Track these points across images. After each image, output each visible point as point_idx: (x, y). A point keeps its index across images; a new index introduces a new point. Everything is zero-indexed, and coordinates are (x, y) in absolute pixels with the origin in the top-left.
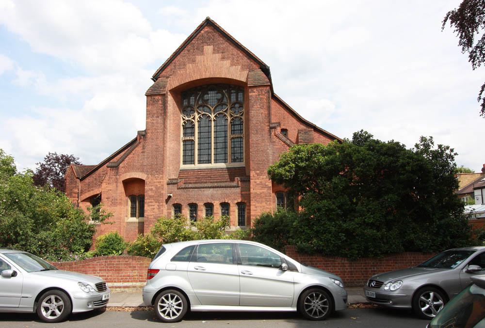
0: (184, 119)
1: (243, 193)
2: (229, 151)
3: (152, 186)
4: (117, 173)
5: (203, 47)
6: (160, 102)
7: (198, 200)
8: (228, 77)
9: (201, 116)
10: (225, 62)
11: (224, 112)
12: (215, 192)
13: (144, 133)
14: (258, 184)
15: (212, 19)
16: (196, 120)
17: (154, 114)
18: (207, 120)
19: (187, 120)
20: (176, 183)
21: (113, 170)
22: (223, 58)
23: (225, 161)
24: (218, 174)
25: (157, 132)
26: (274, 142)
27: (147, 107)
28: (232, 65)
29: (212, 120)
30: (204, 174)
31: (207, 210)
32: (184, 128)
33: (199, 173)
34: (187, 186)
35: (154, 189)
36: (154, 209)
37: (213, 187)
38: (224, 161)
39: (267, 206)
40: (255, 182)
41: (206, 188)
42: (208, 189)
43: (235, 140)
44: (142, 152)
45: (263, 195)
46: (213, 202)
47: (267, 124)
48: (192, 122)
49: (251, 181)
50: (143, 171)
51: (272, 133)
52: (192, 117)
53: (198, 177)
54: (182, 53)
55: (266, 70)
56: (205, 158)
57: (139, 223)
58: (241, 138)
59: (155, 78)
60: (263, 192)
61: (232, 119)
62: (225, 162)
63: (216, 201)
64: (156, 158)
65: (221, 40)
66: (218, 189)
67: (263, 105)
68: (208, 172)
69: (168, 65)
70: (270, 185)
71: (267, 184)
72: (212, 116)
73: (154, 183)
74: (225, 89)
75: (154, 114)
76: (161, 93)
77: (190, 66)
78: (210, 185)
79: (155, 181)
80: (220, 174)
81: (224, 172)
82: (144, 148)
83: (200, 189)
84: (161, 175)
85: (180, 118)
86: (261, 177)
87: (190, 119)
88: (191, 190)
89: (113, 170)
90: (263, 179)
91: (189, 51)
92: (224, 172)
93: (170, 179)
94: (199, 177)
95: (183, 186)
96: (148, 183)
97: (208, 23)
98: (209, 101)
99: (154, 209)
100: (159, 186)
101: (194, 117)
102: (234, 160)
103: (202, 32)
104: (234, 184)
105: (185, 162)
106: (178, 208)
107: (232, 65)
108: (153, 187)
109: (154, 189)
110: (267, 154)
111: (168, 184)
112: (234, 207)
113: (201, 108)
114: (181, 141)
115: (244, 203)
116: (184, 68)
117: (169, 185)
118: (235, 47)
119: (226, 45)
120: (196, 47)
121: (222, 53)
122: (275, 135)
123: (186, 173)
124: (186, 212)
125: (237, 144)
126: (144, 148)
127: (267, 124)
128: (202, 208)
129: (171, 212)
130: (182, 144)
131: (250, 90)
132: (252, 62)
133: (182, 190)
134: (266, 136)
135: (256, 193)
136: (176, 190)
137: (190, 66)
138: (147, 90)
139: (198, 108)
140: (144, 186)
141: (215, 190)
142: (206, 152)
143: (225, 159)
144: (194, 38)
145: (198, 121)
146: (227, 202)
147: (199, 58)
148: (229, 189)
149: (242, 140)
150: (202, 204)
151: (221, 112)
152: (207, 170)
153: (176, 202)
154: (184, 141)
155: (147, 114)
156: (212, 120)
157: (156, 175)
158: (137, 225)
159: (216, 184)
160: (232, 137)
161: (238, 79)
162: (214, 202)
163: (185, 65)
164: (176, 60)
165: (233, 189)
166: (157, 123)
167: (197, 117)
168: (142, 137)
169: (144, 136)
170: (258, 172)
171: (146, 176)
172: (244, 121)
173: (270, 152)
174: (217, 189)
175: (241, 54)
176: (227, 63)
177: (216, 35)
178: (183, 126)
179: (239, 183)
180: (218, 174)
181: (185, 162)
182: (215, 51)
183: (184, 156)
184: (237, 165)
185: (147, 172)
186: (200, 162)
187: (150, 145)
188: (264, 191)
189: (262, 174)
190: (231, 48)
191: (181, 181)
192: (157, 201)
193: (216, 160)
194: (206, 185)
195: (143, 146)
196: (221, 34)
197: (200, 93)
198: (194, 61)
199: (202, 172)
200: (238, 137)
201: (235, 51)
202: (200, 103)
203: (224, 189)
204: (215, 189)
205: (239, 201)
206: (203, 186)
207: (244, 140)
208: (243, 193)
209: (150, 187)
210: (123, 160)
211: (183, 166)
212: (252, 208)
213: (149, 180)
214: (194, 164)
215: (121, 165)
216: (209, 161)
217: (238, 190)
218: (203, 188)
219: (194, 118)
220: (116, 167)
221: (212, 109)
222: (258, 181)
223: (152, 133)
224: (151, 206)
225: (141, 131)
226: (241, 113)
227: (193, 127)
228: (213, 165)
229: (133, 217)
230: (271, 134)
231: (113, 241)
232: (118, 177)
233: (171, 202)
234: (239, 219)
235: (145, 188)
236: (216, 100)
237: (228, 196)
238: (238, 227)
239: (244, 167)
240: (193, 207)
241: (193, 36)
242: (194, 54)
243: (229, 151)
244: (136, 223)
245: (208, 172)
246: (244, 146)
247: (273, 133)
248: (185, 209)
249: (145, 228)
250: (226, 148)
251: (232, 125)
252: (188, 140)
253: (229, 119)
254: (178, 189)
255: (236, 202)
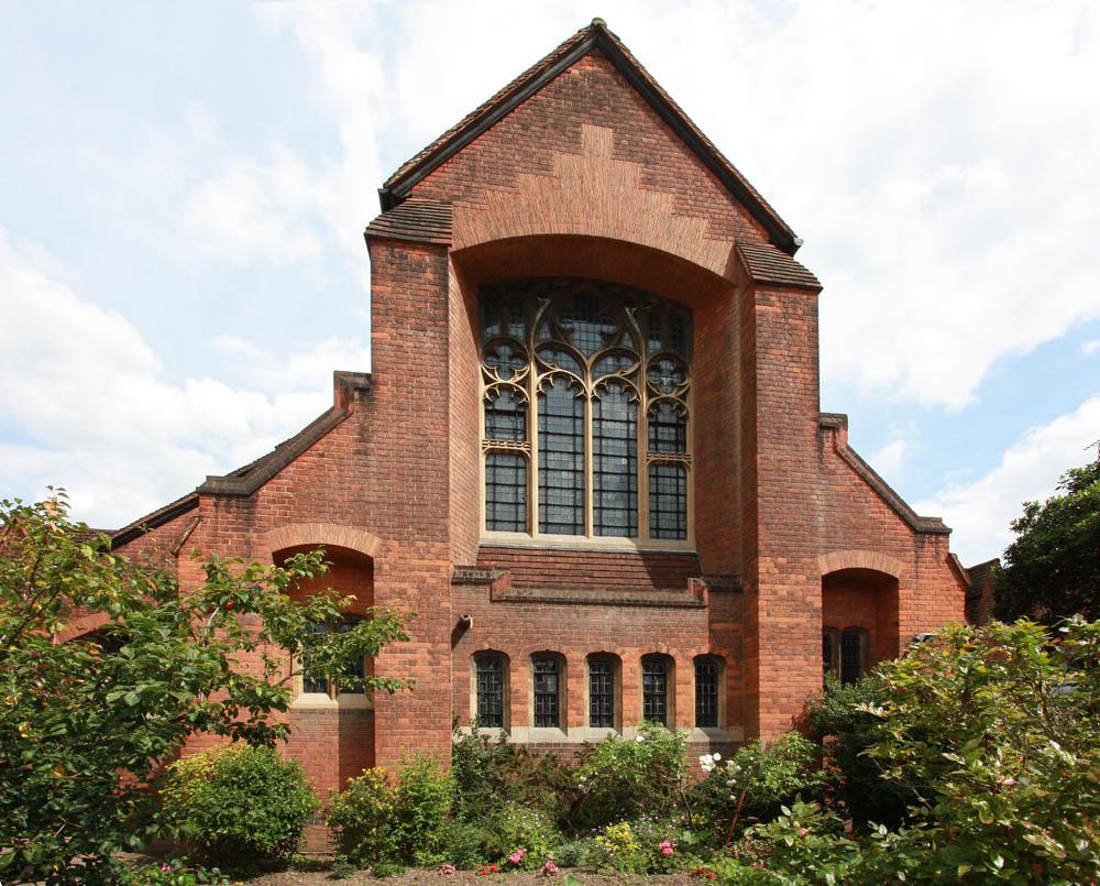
0: (487, 381)
1: (716, 626)
2: (644, 503)
3: (403, 580)
4: (249, 522)
5: (578, 125)
6: (429, 276)
7: (565, 641)
8: (665, 247)
9: (551, 379)
10: (655, 197)
11: (628, 376)
12: (625, 620)
13: (361, 381)
14: (781, 599)
15: (613, 27)
16: (534, 392)
17: (406, 315)
18: (570, 395)
19: (501, 386)
20: (488, 582)
21: (228, 506)
22: (649, 182)
23: (630, 530)
24: (614, 568)
25: (420, 386)
26: (832, 473)
27: (374, 281)
28: (679, 212)
29: (590, 396)
30: (568, 566)
31: (593, 677)
32: (487, 411)
33: (551, 559)
34: (525, 594)
35: (412, 591)
36: (413, 663)
37: (621, 604)
38: (625, 531)
39: (810, 669)
40: (774, 593)
41: (595, 603)
42: (602, 609)
43: (662, 471)
44: (358, 452)
45: (796, 633)
46: (618, 652)
47: (811, 415)
48: (520, 395)
49: (761, 586)
50: (365, 525)
51: (827, 444)
52: (519, 379)
53: (546, 572)
54: (501, 126)
55: (785, 241)
56: (566, 516)
57: (342, 712)
58: (680, 465)
59: (391, 196)
60: (798, 624)
61: (654, 405)
62: (629, 536)
63: (627, 649)
64: (418, 479)
65: (640, 117)
66: (637, 610)
67: (800, 350)
68: (581, 560)
69: (445, 160)
70: (818, 603)
71: (809, 599)
72: (590, 387)
73: (412, 569)
74: (631, 307)
75: (406, 315)
76: (433, 241)
77: (529, 181)
78: (610, 596)
79: (415, 562)
80: (619, 568)
81: (633, 563)
82: (364, 435)
83: (573, 607)
84: (438, 544)
85: (477, 377)
86: (793, 576)
87: (511, 382)
88: (541, 607)
89: (228, 506)
90: (797, 583)
91: (525, 127)
92: (633, 563)
93: (460, 567)
94: (552, 572)
95: (513, 593)
96: (386, 567)
97: (599, 43)
98: (576, 336)
99: (413, 663)
100: (431, 581)
101: (528, 376)
102: (657, 532)
103: (575, 71)
104: (688, 596)
105: (493, 523)
106: (492, 665)
107: (679, 212)
108: (406, 585)
109: (412, 591)
110: (811, 507)
111: (456, 583)
112: (686, 667)
113: (549, 354)
114: (481, 451)
115: (719, 657)
116: (507, 183)
117: (458, 588)
118: (690, 156)
119: (656, 138)
120: (551, 121)
121: (647, 163)
122: (836, 452)
123: (502, 557)
124: (523, 680)
125: (668, 485)
126: (364, 435)
127: (811, 415)
128: (581, 668)
129: (468, 680)
130: (483, 461)
131: (757, 295)
132: (744, 215)
133: (509, 605)
134: (811, 450)
135: (775, 626)
136: (485, 603)
137: (529, 181)
138: (372, 219)
139: (538, 350)
140: (371, 581)
141: (629, 613)
142: (568, 498)
143: (629, 527)
144: (545, 85)
145: (540, 395)
146: (664, 651)
147: (561, 161)
148: (670, 612)
149: (681, 474)
150: (583, 656)
151: (617, 375)
152: (574, 554)
153: (486, 647)
154: (491, 453)
155: (374, 312)
156: (590, 396)
157: (419, 544)
158: (337, 721)
159: (626, 595)
160: (653, 459)
161: (700, 263)
162: (623, 652)
163: (509, 171)
164: (477, 146)
165: (683, 611)
166: (418, 350)
167: (536, 380)
168: (356, 395)
169: (363, 391)
170: (781, 560)
171: (377, 541)
172: (691, 415)
173: (818, 499)
174: (631, 610)
175: (708, 183)
176: (662, 202)
177: (625, 96)
178: (486, 402)
179: (706, 594)
180: (614, 568)
181: (493, 523)
182: (623, 151)
183: (492, 502)
184: (669, 546)
185: (381, 530)
186: (546, 526)
187: (390, 433)
188: (798, 620)
189: (794, 568)
190: (677, 155)
191: (500, 578)
192: (429, 637)
193: (601, 526)
194: (592, 595)
195: (363, 430)
196: (643, 95)
197: (548, 302)
198: (544, 168)
199: (559, 560)
200: (670, 464)
201: (690, 168)
202: (543, 336)
203: (657, 611)
204: (625, 609)
205: (705, 650)
206: (584, 597)
207: (690, 475)
208: (716, 626)
209: (396, 585)
210: (274, 475)
211: (488, 537)
212: (764, 671)
213: (392, 557)
214: (529, 531)
215: (264, 490)
216: (577, 528)
217: (700, 617)
218: (586, 603)
219: (526, 382)
220: (245, 496)
221: (589, 363)
222: (783, 590)
223: (397, 384)
224: (402, 651)
225: (348, 374)
226: (681, 388)
227: (522, 412)
228: (591, 541)
229: (309, 692)
230: (820, 449)
231: (264, 778)
232: (253, 536)
233: (469, 645)
234: (698, 708)
235: (376, 584)
236: (598, 338)
237: (667, 633)
238: (698, 730)
239: (694, 555)
240: (549, 664)
241: (542, 72)
242: (544, 141)
243: (644, 503)
244: (331, 711)
245: (581, 560)
246: (690, 492)
247: (828, 445)
248: (521, 668)
249: (378, 732)
250: (630, 492)
251: (650, 424)
252: (503, 452)
253: (645, 402)
254: (492, 601)
255: (694, 653)
